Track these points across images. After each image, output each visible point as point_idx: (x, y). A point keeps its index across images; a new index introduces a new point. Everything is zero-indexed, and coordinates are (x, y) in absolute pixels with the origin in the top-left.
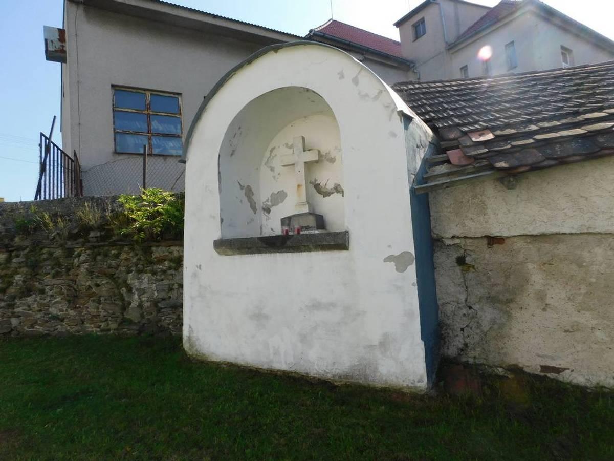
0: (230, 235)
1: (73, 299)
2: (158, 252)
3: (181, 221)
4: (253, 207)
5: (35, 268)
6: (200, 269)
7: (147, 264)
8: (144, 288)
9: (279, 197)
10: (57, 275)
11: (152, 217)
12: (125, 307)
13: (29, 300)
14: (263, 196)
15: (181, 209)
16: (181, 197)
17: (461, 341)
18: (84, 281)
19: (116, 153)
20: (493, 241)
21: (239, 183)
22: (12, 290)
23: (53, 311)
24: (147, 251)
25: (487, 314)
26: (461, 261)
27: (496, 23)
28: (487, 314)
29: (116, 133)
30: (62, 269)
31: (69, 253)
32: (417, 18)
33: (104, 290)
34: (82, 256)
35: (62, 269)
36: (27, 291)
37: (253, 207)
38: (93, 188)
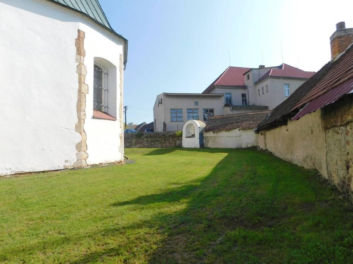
0: (187, 136)
1: (170, 144)
2: (180, 138)
3: (182, 135)
4: (189, 133)
5: (165, 140)
6: (11, 169)
7: (178, 140)
8: (178, 142)
9: (192, 132)
10: (168, 141)
11: (179, 134)
12: (176, 144)
13: (164, 144)
14: (190, 132)
15: (182, 133)
16: (182, 132)
17: (319, 161)
18: (171, 142)
19: (171, 121)
20: (207, 137)
21: (115, 205)
22: (162, 143)
23: (167, 145)
24: (178, 138)
25: (207, 143)
26: (205, 139)
27: (263, 80)
28: (207, 143)
29: (171, 117)
30: (168, 140)
31: (169, 138)
32: (248, 74)
33: (173, 143)
34: (171, 138)
35: (168, 140)
36: (164, 143)
37: (189, 133)
38: (168, 129)
